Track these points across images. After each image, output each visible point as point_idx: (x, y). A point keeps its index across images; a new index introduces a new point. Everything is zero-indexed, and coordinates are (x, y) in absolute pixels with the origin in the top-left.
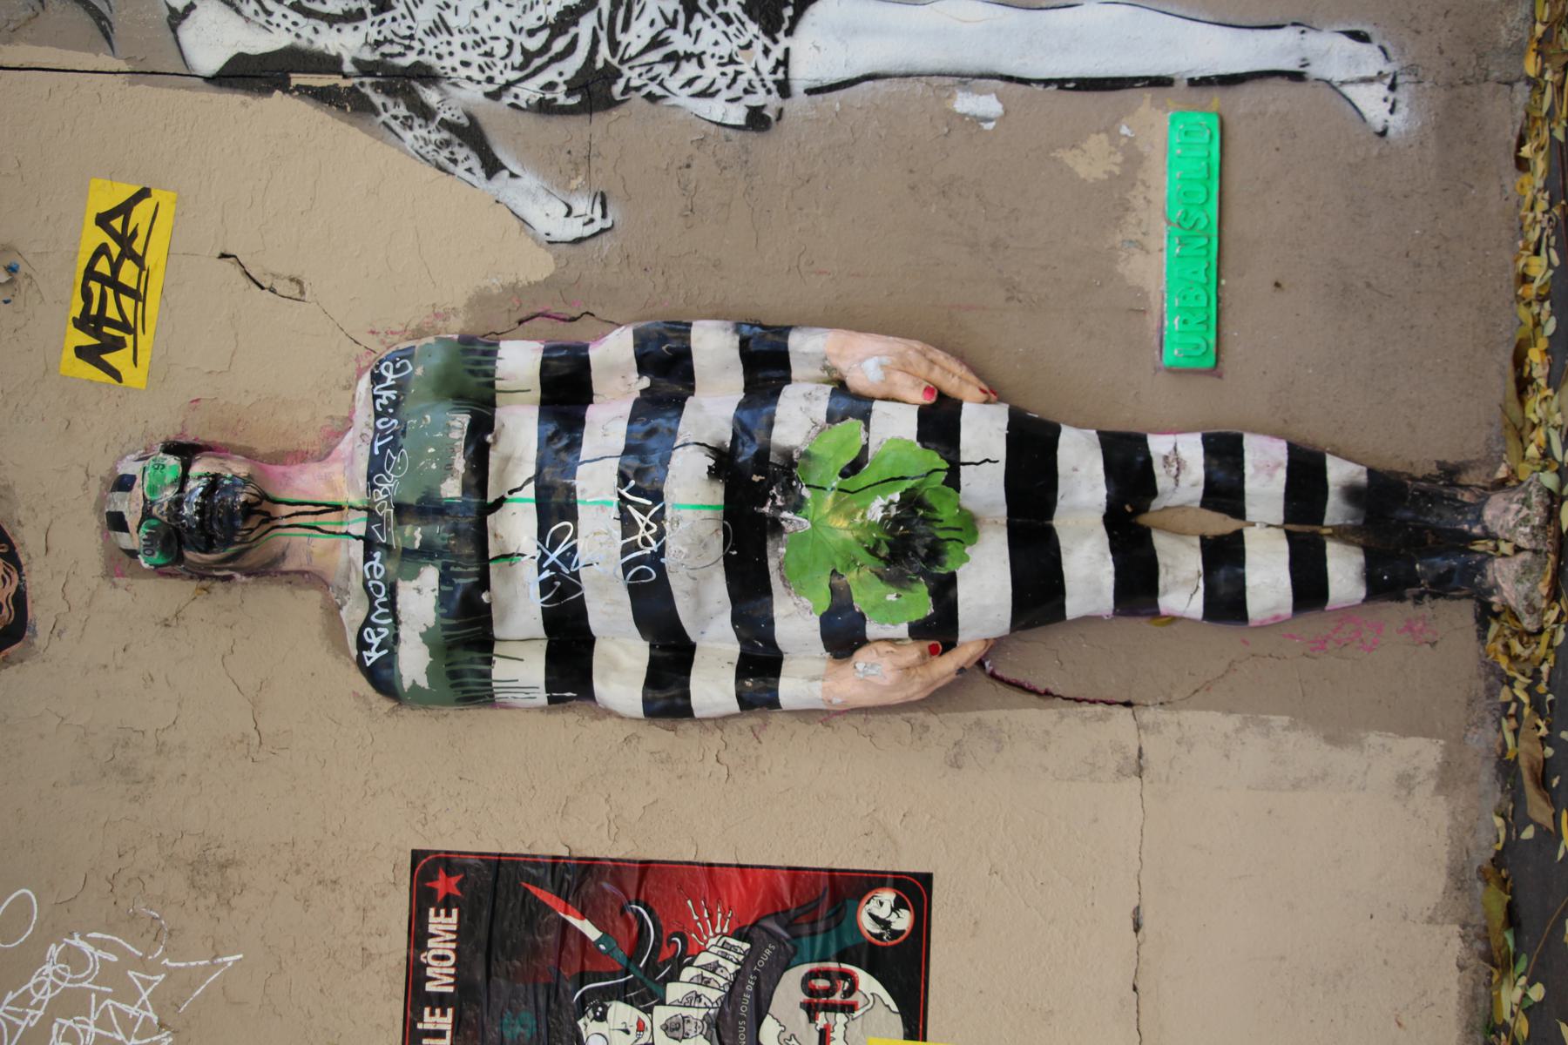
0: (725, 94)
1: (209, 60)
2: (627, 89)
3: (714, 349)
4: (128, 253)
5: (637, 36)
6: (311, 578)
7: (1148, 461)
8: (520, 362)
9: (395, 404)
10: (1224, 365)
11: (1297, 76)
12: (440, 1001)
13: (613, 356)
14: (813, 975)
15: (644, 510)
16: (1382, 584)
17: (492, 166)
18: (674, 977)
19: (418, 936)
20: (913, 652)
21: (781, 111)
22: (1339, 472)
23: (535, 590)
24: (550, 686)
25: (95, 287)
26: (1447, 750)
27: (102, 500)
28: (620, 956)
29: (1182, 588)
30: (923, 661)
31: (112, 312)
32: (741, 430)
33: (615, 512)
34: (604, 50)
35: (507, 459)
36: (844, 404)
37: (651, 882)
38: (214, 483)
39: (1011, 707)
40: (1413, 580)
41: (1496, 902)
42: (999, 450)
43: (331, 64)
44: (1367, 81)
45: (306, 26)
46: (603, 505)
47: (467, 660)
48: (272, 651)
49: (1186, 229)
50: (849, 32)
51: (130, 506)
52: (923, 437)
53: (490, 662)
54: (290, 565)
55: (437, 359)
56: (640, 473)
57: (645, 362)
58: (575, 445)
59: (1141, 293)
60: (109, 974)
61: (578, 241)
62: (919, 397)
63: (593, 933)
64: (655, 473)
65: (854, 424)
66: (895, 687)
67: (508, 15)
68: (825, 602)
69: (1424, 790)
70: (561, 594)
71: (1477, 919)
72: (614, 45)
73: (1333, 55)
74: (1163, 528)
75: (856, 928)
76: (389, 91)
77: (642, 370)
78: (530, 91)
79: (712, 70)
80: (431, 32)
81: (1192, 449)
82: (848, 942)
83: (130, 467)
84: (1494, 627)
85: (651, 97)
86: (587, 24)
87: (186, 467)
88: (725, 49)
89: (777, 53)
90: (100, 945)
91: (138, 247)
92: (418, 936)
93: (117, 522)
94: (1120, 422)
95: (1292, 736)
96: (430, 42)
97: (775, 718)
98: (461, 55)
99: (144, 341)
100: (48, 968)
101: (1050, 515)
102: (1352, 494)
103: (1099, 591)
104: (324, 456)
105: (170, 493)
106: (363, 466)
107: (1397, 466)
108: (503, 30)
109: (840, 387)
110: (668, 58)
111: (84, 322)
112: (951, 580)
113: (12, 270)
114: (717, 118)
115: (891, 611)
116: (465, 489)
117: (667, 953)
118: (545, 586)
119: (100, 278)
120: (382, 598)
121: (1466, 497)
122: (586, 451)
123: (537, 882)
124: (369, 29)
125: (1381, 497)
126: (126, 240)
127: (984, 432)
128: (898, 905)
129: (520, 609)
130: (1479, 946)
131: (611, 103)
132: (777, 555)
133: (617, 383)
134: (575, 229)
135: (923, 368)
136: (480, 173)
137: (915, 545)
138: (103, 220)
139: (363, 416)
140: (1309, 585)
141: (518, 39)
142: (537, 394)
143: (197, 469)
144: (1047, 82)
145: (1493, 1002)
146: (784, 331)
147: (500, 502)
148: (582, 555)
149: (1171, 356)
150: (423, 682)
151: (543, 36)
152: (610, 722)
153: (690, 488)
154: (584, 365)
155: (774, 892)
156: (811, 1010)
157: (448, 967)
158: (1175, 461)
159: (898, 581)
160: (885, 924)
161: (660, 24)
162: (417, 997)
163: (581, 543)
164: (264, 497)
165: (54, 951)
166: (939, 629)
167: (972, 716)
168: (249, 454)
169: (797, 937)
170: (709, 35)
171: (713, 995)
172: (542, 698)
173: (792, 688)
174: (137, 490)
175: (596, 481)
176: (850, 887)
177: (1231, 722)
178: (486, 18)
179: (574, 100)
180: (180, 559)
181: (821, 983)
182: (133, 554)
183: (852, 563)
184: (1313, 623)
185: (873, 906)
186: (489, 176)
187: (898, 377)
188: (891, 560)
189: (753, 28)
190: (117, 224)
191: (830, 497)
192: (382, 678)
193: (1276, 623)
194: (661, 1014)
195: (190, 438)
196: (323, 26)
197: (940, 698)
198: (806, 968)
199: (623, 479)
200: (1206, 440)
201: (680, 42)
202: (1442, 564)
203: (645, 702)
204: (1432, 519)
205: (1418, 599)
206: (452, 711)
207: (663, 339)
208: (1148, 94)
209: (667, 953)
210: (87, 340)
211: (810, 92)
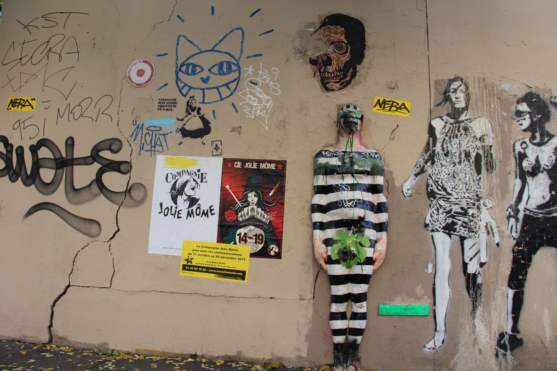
0: (431, 219)
1: (434, 123)
2: (432, 201)
3: (383, 217)
4: (398, 108)
5: (442, 202)
6: (338, 141)
7: (362, 302)
8: (380, 180)
9: (371, 157)
10: (380, 317)
11: (436, 330)
12: (258, 166)
13: (381, 198)
14: (262, 236)
15: (353, 204)
16: (337, 346)
17: (416, 175)
18: (262, 210)
19: (270, 162)
20: (325, 256)
21: (428, 230)
22: (359, 338)
23: (337, 183)
24: (318, 186)
25: (391, 103)
26: (305, 357)
27: (352, 104)
28: (266, 199)
29: (336, 308)
30: (323, 258)
31: (386, 106)
32: (368, 223)
33: (352, 198)
34: (439, 196)
35: (362, 178)
36: (373, 242)
37: (280, 205)
38: (356, 124)
39: (313, 275)
40: (338, 352)
41: (276, 366)
42: (364, 273)
43: (434, 145)
44: (435, 344)
45: (441, 141)
46: (353, 196)
47: (323, 170)
48: (323, 133)
49: (406, 309)
50: (444, 243)
51: (352, 109)
52: (367, 257)
53: (322, 175)
54: (340, 138)
55: (380, 165)
56: (359, 203)
57: (380, 204)
58: (365, 191)
59: (394, 300)
60: (265, 107)
61: (403, 191)
62: (374, 257)
63: (270, 194)
64: (360, 206)
65: (369, 244)
66: (318, 251)
67: (445, 178)
68: (334, 239)
69: (297, 353)
70: (336, 188)
71: (273, 362)
72: (440, 198)
73: (439, 337)
74: (348, 304)
75: (271, 244)
76: (430, 156)
77: (378, 204)
78: (431, 182)
79: (436, 217)
80: (441, 164)
81: (364, 310)
82: (269, 243)
83: (358, 109)
84: (328, 367)
85: (430, 205)
86: (444, 193)
87: (359, 119)
88: (440, 219)
89: (439, 229)
90: (270, 105)
91: (399, 110)
92: (270, 162)
93: (348, 107)
94: (369, 296)
95: (307, 329)
96: (439, 164)
97: (311, 229)
98: (437, 169)
99: (381, 111)
100: (266, 97)
101: (351, 282)
102: (355, 341)
103: (336, 292)
104: (361, 144)
105: (354, 116)
106: (360, 151)
107: (360, 349)
108: (442, 177)
109: (376, 242)
110: (438, 208)
111: (384, 101)
112: (339, 263)
113: (393, 88)
114: (427, 218)
115: (333, 251)
116: (356, 170)
117: (267, 208)
118: (337, 185)
119: (393, 104)
120: (335, 154)
121: (354, 363)
122: (363, 193)
123: (281, 183)
124: (441, 152)
125: (354, 346)
126: (400, 108)
127: (368, 270)
128: (275, 252)
129: (333, 180)
130: (267, 362)
131: (429, 198)
132: (344, 229)
133: (376, 199)
134: (405, 191)
135: (380, 258)
136: (415, 173)
137: (346, 256)
138: (403, 104)
139: (369, 151)
140: (337, 332)
141: (440, 180)
142: (373, 183)
143: (359, 121)
144: (434, 282)
145: (257, 364)
146: (386, 231)
147: (353, 176)
148: (343, 192)
149: (382, 306)
150: (318, 162)
151: (441, 185)
152: (310, 197)
153: (357, 213)
154: (379, 192)
155: (278, 228)
156: (256, 235)
157: (265, 167)
158: (361, 307)
159: (339, 253)
160: (272, 250)
161: (444, 207)
162: (259, 162)
163: (346, 192)
164: (354, 133)
165: (269, 98)
166: (329, 261)
167: (311, 267)
168: (361, 130)
169: (269, 233)
170: (442, 216)
171: (259, 217)
172: (315, 185)
173: (317, 232)
174: (354, 110)
175: (358, 195)
176: (279, 243)
177: (310, 317)
178: (444, 174)
179: (429, 190)
180: (342, 118)
181: (261, 237)
182: (342, 109)
183: (342, 244)
184: (329, 333)
185: (275, 247)
186: (415, 174)
187: (378, 253)
188: (343, 252)
189: (444, 225)
190: (403, 107)
191: (355, 240)
192: (319, 155)
193: (329, 326)
194: (255, 207)
195: (364, 120)
196: (441, 144)
197: (315, 261)
198: (264, 235)
199: (358, 200)
200: (366, 313)
201: (441, 211)
202: (341, 358)
203: (315, 204)
204: (350, 356)
205: (334, 353)
206: (313, 167)
207: (384, 207)
208: (432, 301)
209: (267, 208)
210: (381, 101)
211: (432, 236)
